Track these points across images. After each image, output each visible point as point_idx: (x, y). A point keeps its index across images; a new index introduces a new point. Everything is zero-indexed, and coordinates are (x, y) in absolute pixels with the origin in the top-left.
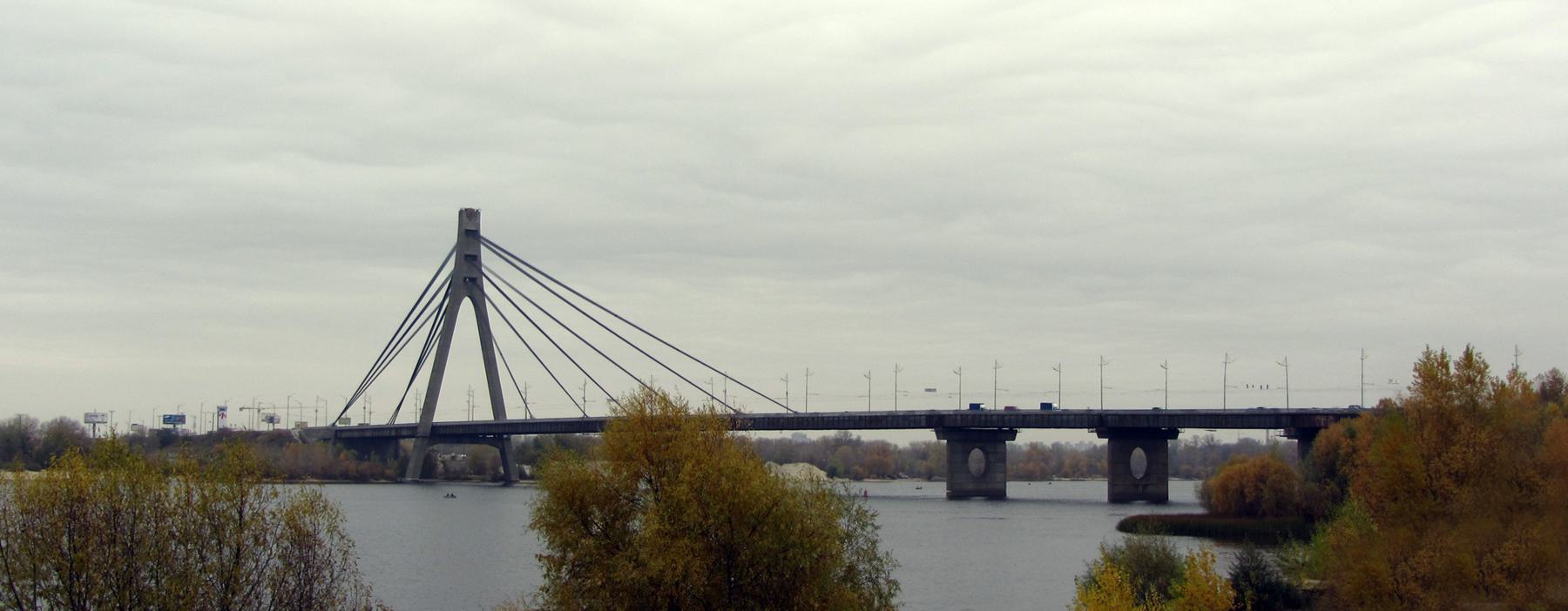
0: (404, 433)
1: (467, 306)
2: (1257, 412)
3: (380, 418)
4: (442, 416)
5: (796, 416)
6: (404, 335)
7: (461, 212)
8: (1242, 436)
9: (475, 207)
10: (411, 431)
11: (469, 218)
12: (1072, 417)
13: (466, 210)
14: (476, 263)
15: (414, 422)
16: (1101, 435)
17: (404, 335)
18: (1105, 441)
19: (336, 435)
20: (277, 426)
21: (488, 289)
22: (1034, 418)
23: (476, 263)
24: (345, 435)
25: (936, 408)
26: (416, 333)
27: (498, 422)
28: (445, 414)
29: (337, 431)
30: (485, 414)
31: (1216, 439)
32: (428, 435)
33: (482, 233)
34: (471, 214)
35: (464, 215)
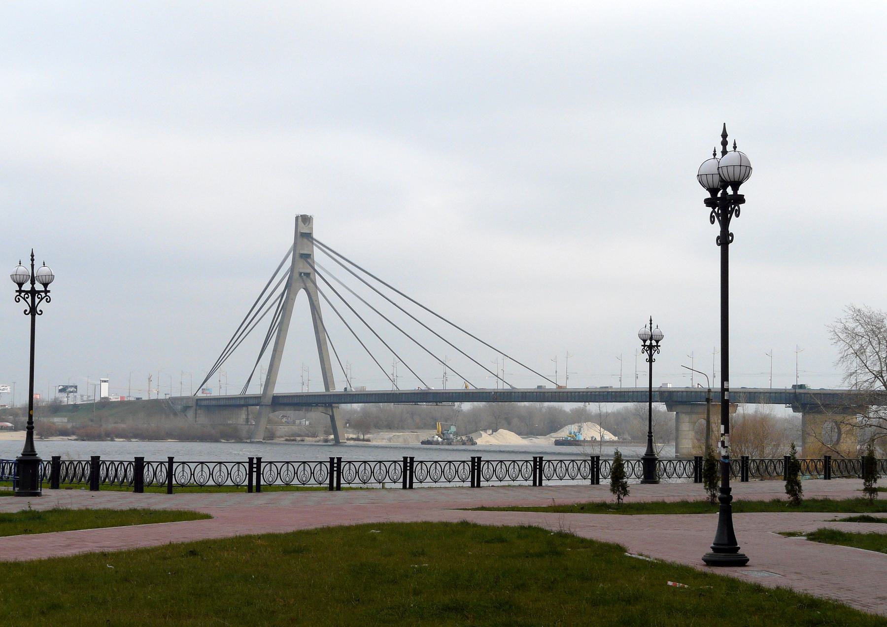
0: (251, 402)
1: (302, 297)
2: (819, 392)
3: (234, 390)
4: (281, 388)
5: (514, 391)
6: (234, 343)
7: (297, 218)
8: (626, 405)
9: (309, 214)
10: (256, 401)
11: (305, 219)
12: (606, 393)
13: (301, 216)
14: (309, 261)
15: (190, 395)
16: (795, 409)
17: (234, 343)
18: (799, 415)
19: (197, 404)
20: (211, 395)
21: (319, 282)
22: (788, 395)
23: (309, 261)
24: (205, 403)
25: (826, 388)
26: (240, 342)
27: (327, 393)
28: (284, 386)
29: (197, 400)
30: (317, 387)
31: (791, 410)
32: (270, 404)
33: (315, 236)
34: (306, 218)
35: (300, 220)
